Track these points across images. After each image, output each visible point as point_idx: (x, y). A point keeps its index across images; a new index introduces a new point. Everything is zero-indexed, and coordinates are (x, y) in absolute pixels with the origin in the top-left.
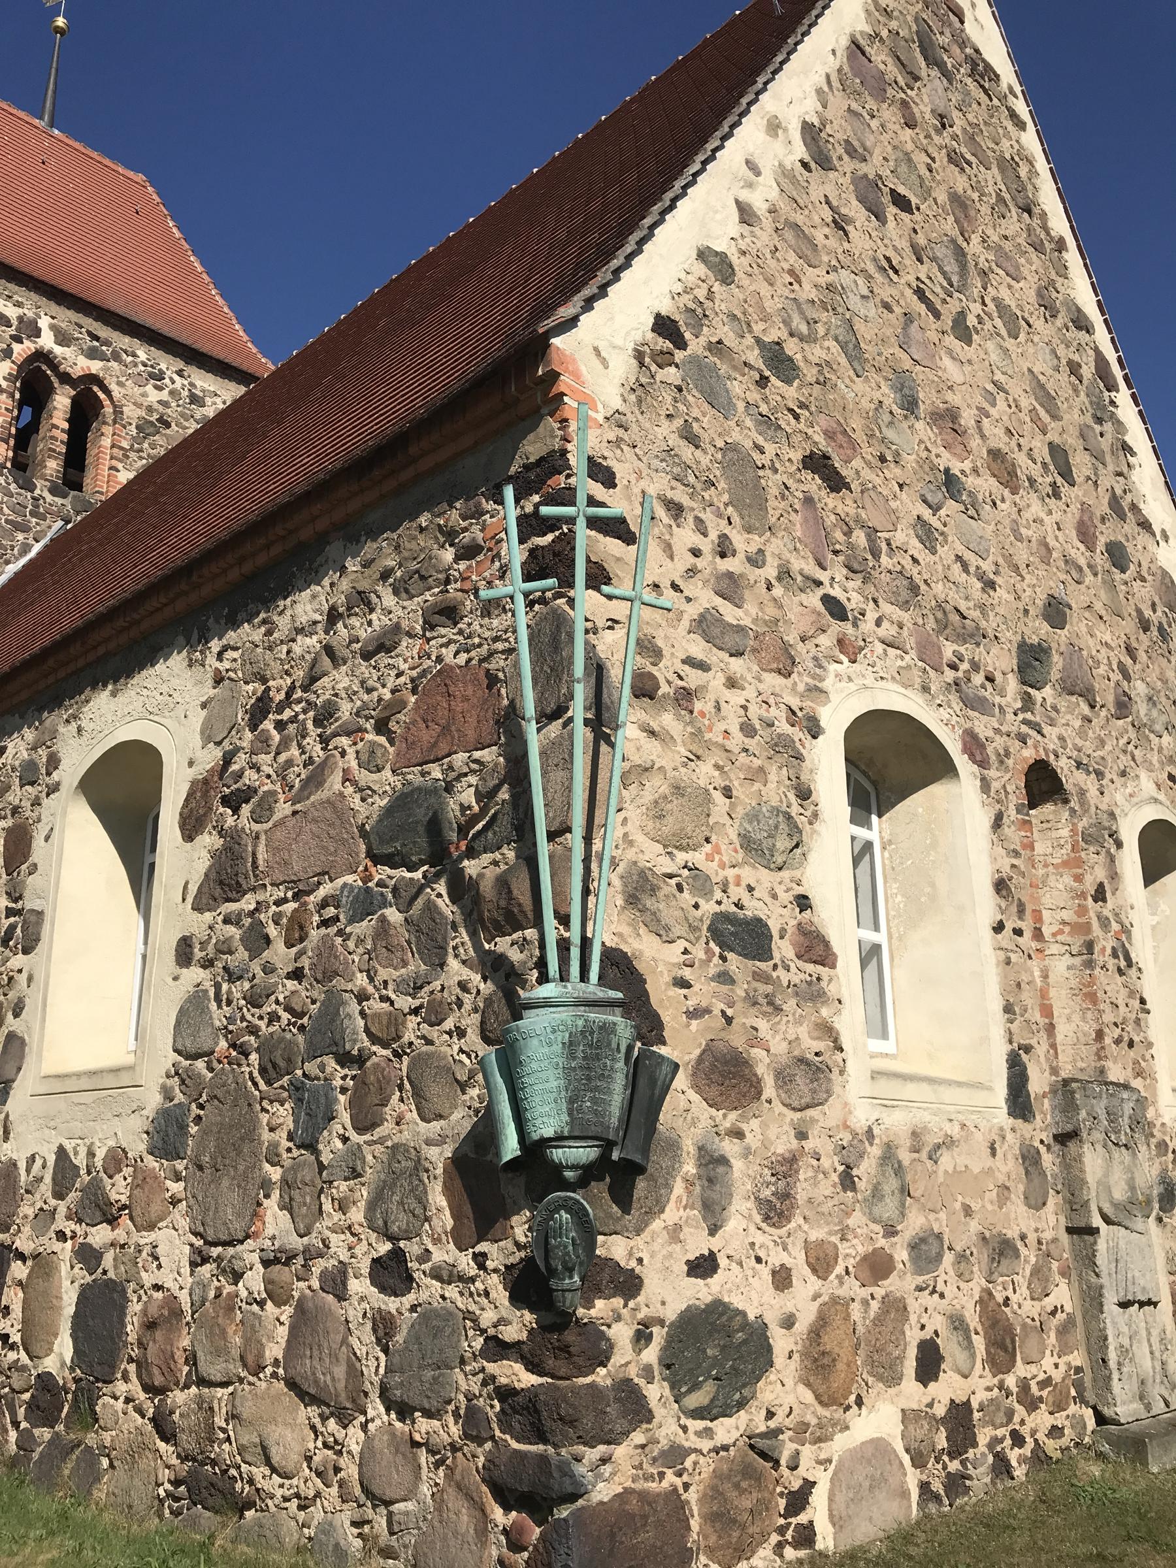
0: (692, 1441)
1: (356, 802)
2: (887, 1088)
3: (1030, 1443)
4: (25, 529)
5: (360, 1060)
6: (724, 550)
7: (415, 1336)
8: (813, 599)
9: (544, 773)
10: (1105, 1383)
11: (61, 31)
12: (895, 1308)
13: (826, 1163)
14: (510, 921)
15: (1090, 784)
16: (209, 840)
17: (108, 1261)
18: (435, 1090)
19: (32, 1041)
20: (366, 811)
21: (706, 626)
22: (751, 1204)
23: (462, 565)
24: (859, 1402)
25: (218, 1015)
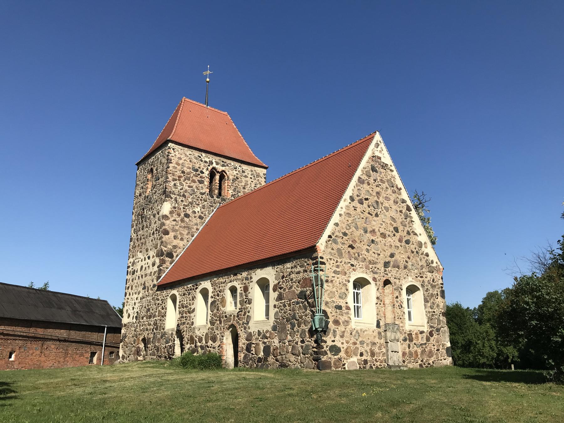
1: (296, 291)
2: (357, 324)
3: (376, 366)
4: (212, 206)
5: (298, 320)
6: (337, 262)
7: (305, 347)
8: (349, 265)
9: (316, 292)
10: (388, 360)
11: (208, 82)
12: (357, 348)
13: (348, 332)
14: (314, 307)
15: (397, 281)
16: (277, 293)
17: (267, 343)
18: (306, 323)
19: (252, 316)
20: (298, 292)
21: (335, 272)
23: (307, 266)
24: (352, 357)
25: (280, 314)
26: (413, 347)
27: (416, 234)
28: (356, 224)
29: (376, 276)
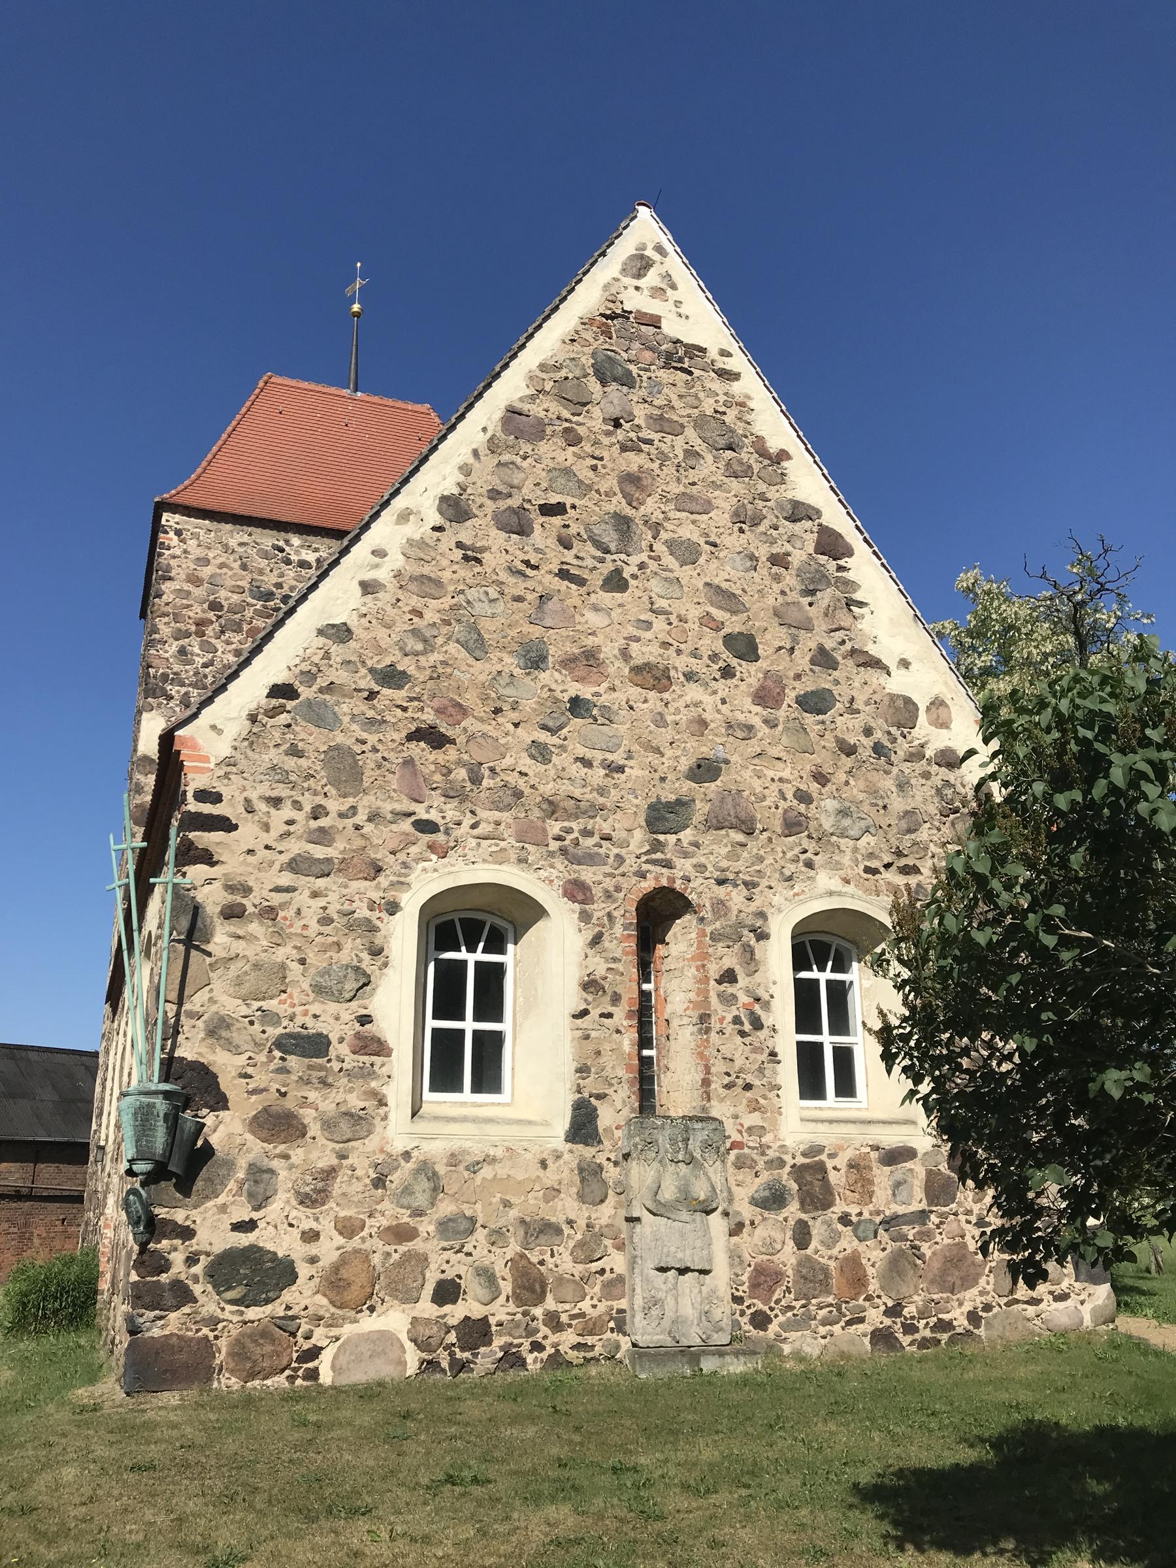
0: (226, 1315)
8: (406, 825)
15: (736, 897)
22: (290, 1195)
26: (832, 1240)
27: (875, 663)
28: (474, 628)
29: (588, 874)
